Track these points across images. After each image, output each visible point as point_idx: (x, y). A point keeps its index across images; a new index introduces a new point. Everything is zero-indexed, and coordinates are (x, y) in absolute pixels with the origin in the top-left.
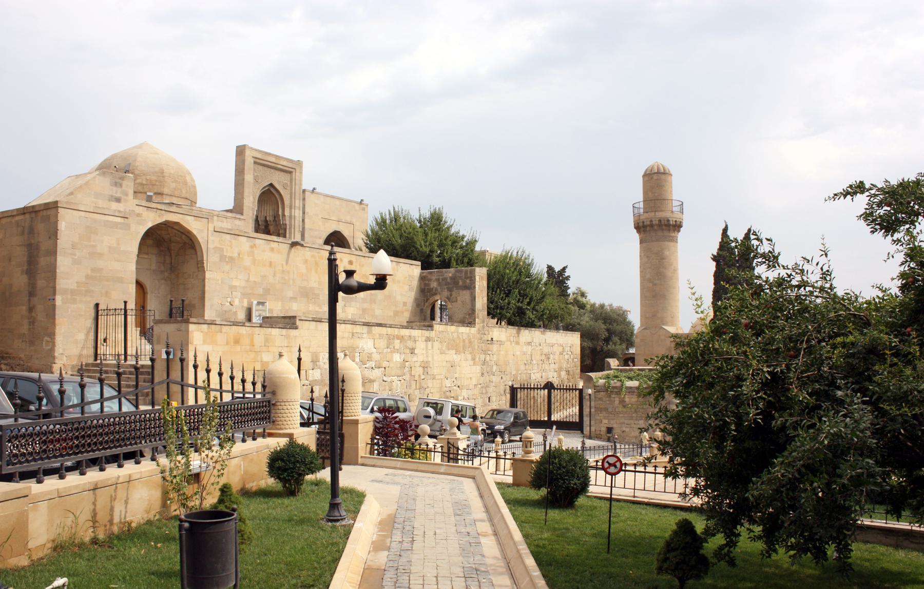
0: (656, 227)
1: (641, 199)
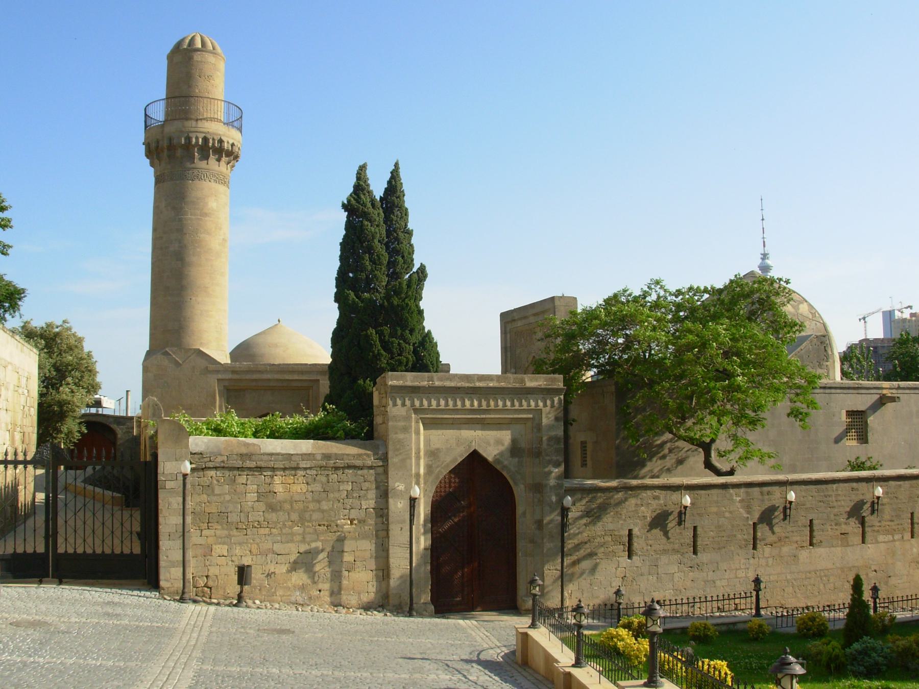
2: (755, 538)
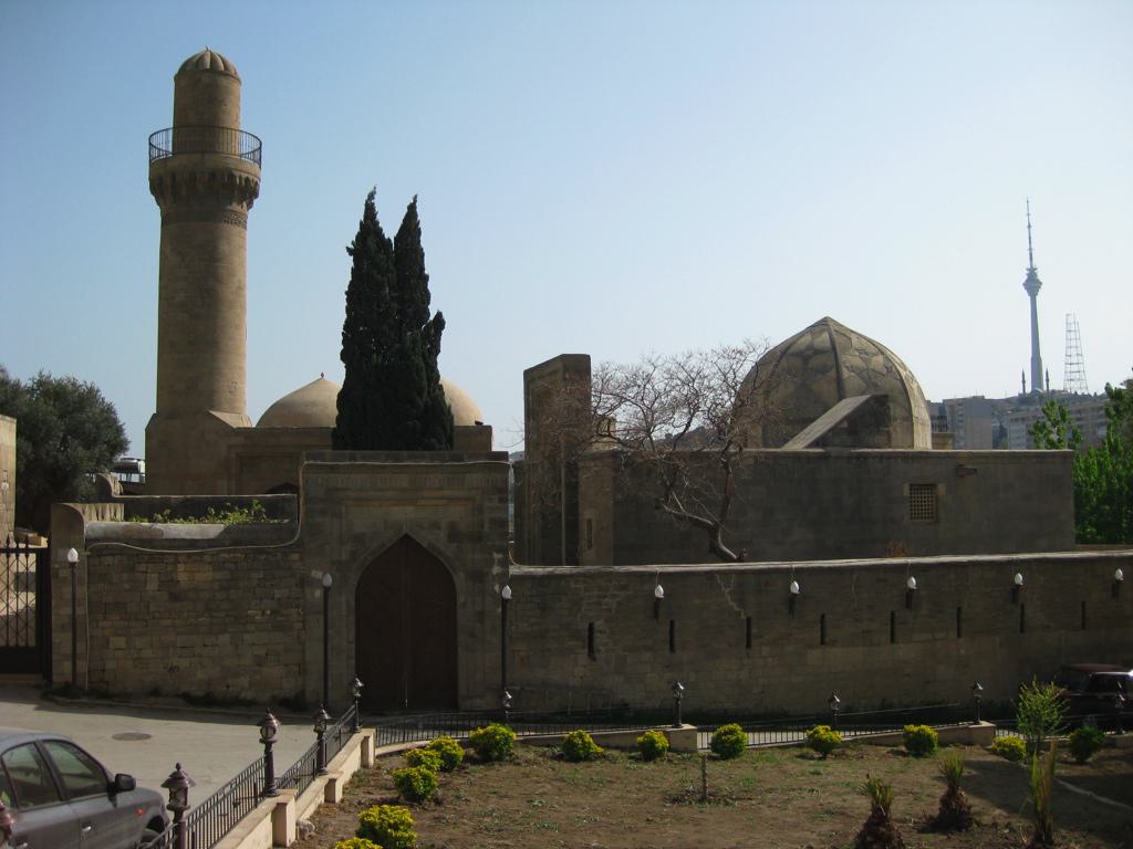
0: (201, 187)
1: (170, 123)
2: (749, 635)
